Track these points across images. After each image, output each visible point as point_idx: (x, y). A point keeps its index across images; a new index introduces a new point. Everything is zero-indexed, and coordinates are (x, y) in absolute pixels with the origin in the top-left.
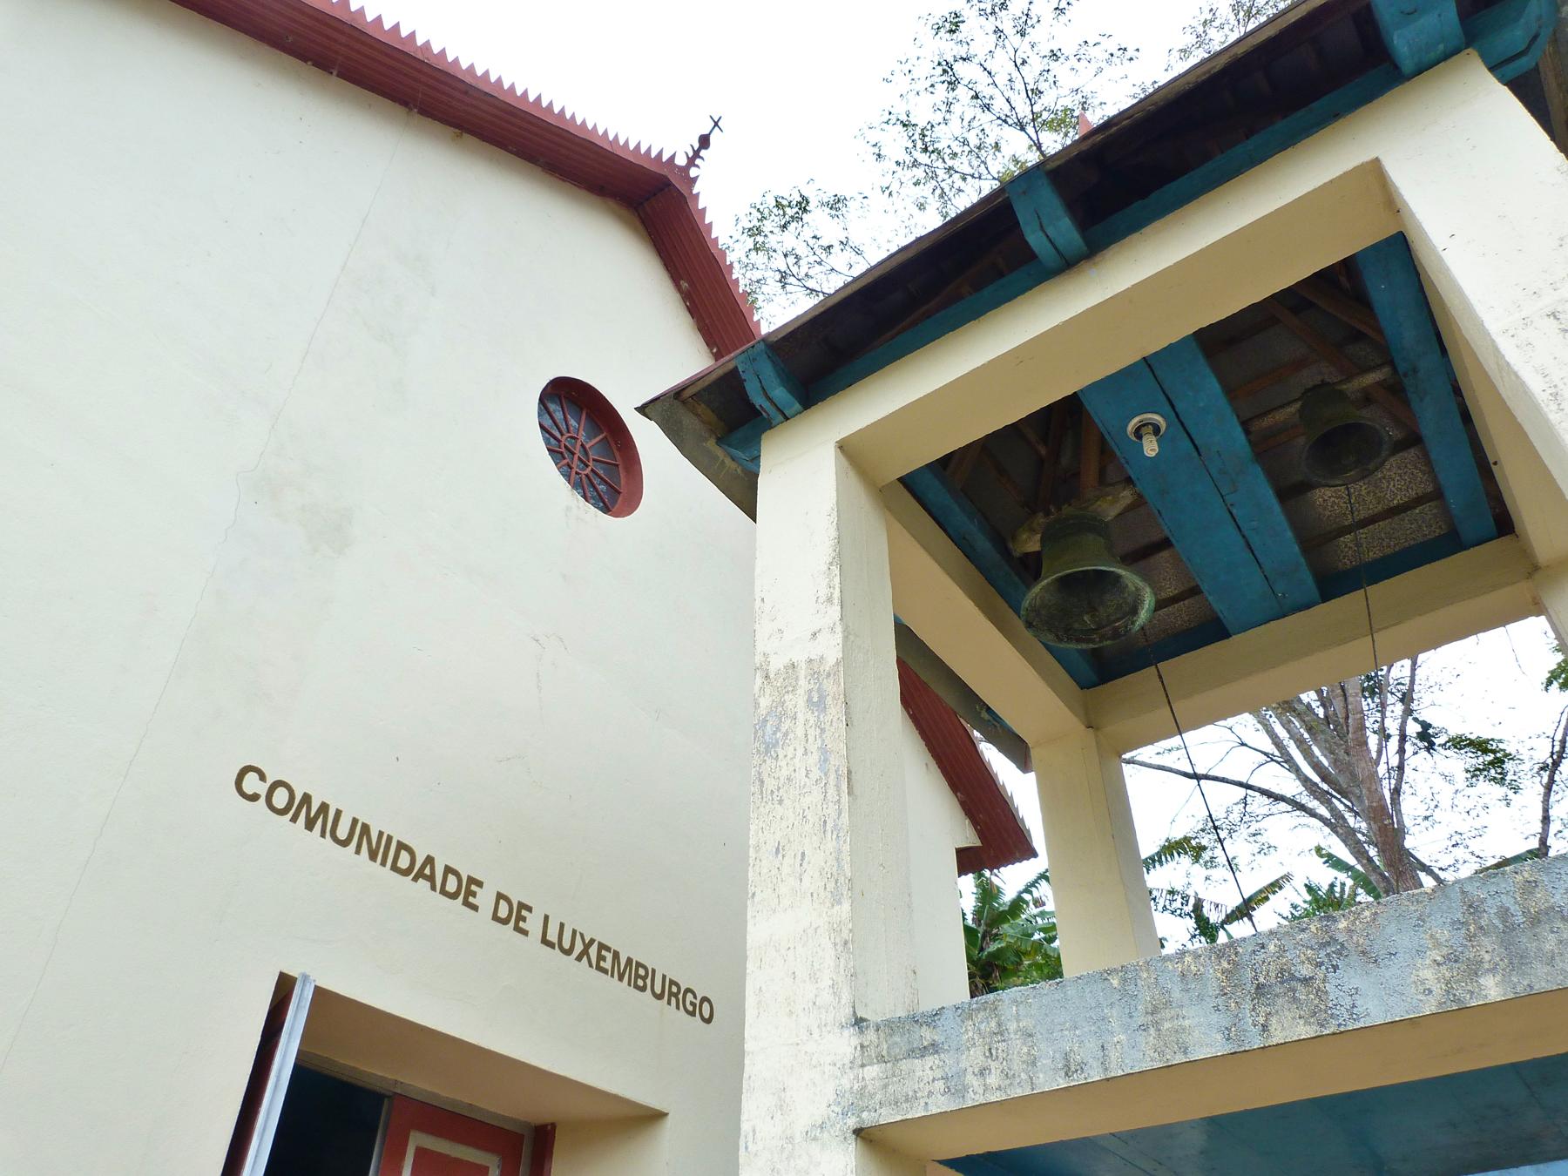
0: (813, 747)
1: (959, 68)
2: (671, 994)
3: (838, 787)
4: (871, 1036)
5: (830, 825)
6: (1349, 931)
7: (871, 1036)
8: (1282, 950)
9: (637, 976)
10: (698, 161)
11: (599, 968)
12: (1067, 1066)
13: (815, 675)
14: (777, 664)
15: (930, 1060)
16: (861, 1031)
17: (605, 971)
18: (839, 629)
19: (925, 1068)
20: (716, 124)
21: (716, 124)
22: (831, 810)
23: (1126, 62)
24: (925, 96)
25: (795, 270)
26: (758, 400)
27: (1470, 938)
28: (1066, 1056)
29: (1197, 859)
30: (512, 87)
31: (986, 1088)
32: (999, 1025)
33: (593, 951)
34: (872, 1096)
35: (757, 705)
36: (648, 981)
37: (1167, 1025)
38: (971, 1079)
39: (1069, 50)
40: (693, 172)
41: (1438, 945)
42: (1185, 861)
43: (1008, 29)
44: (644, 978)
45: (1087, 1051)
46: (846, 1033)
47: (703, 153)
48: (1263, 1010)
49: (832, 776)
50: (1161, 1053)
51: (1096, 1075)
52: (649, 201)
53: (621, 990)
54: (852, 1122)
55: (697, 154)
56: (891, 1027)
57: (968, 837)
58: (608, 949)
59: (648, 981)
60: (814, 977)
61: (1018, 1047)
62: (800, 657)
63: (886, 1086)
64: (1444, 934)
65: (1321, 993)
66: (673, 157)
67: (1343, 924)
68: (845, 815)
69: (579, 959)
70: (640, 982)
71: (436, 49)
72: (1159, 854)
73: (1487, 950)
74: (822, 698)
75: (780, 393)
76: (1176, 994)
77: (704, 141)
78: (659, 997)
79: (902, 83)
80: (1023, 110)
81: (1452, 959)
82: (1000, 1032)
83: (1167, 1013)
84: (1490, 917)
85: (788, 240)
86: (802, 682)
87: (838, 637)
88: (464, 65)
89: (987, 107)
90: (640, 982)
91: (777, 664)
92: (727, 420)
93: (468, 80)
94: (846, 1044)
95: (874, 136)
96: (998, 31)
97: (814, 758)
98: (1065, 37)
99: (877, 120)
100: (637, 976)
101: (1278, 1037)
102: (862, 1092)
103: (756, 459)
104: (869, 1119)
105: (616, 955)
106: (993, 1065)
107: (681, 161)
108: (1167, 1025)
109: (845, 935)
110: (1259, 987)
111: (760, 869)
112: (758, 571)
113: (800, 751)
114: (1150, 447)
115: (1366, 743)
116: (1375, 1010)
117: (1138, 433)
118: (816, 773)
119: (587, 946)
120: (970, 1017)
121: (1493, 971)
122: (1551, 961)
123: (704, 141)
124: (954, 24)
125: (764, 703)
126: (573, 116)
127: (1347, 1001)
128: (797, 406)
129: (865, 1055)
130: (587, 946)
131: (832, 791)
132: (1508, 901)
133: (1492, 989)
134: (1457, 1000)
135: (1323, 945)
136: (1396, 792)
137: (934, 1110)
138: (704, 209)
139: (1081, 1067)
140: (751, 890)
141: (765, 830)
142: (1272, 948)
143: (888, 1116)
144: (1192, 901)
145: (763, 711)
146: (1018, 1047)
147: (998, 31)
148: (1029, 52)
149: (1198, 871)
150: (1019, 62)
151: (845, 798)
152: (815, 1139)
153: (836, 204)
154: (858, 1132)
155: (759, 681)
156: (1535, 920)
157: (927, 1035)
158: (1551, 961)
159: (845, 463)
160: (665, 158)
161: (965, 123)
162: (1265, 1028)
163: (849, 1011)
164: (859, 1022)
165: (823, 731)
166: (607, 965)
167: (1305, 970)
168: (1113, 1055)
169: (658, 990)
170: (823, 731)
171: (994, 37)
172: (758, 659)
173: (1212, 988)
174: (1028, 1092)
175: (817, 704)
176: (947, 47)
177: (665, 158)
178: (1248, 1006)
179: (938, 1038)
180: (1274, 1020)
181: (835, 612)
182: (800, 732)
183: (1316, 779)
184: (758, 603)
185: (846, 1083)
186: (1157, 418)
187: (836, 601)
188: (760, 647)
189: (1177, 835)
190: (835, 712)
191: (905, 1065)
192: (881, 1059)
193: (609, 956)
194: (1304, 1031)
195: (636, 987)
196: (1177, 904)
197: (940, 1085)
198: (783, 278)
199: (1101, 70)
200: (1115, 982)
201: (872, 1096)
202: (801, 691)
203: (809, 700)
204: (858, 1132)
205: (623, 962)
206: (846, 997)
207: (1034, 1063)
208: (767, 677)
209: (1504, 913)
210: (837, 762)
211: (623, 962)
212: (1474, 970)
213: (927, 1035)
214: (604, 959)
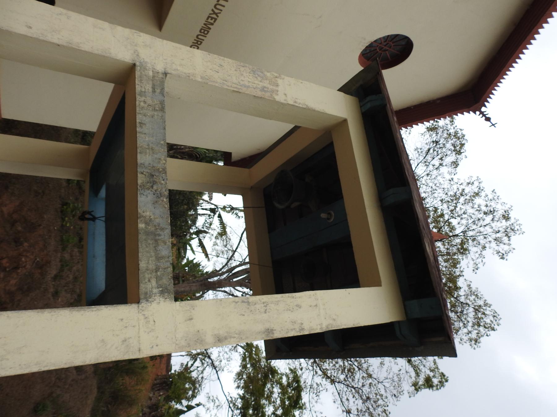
0: (250, 84)
1: (491, 216)
2: (198, 41)
3: (236, 88)
4: (161, 76)
5: (225, 82)
6: (163, 201)
7: (161, 76)
8: (162, 184)
9: (205, 30)
10: (481, 115)
11: (209, 17)
12: (142, 123)
13: (273, 91)
14: (280, 81)
15: (151, 90)
16: (163, 74)
17: (208, 19)
18: (285, 102)
19: (148, 87)
20: (493, 125)
21: (493, 125)
22: (230, 84)
23: (473, 269)
24: (485, 203)
25: (438, 146)
26: (368, 98)
27: (155, 226)
28: (145, 124)
29: (219, 233)
30: (527, 49)
31: (140, 101)
32: (157, 110)
33: (214, 16)
34: (144, 71)
35: (268, 72)
36: (202, 34)
37: (148, 151)
38: (143, 99)
39: (484, 253)
40: (478, 113)
41: (155, 218)
42: (219, 230)
43: (498, 235)
44: (204, 33)
45: (145, 129)
46: (163, 69)
47: (484, 118)
48: (147, 174)
49: (240, 87)
50: (141, 147)
51: (138, 129)
52: (472, 94)
53: (201, 24)
54: (138, 64)
55: (484, 115)
56: (162, 82)
57: (235, 157)
58: (215, 22)
59: (202, 34)
60: (181, 65)
61: (150, 113)
62: (280, 88)
63: (146, 76)
64: (157, 221)
65: (148, 189)
66: (485, 106)
67: (165, 200)
68: (227, 87)
69: (213, 10)
70: (202, 31)
71: (549, 20)
72: (223, 222)
73: (151, 228)
74: (265, 91)
75: (368, 106)
76: (155, 156)
77: (488, 119)
78: (197, 37)
79: (490, 197)
80: (470, 233)
81: (151, 220)
82: (155, 110)
83: (151, 152)
84: (159, 232)
85: (449, 146)
86: (271, 87)
87: (282, 101)
88: (540, 30)
89: (474, 222)
90: (202, 31)
91: (280, 81)
92: (366, 89)
93: (534, 31)
94: (160, 68)
95: (476, 184)
96: (499, 232)
97: (247, 84)
98: (487, 253)
99: (482, 185)
100: (205, 30)
101: (139, 175)
102: (145, 69)
103: (352, 95)
104: (138, 68)
105: (212, 24)
106: (146, 105)
107: (483, 109)
108: (148, 151)
109: (191, 77)
110: (153, 176)
111: (217, 59)
112: (312, 84)
113: (250, 80)
114: (323, 216)
115: (241, 286)
116: (142, 199)
117: (329, 214)
118: (242, 83)
119: (216, 14)
120: (160, 103)
121: (146, 227)
122: (145, 240)
123: (488, 119)
124: (506, 217)
125: (268, 74)
126: (510, 71)
127: (145, 194)
128: (363, 110)
129: (156, 73)
130: (216, 14)
131: (235, 86)
132: (162, 237)
133: (141, 226)
134: (140, 217)
135: (161, 194)
136: (225, 292)
137: (137, 86)
138: (463, 114)
139: (141, 127)
140: (211, 55)
141: (229, 64)
142: (163, 182)
143: (137, 74)
144: (207, 230)
145: (266, 73)
146: (150, 113)
147: (499, 232)
148: (488, 240)
149: (215, 234)
150: (486, 236)
151: (232, 89)
152: (135, 52)
153: (455, 164)
154: (134, 65)
155: (276, 75)
156: (156, 241)
157: (158, 91)
158: (145, 240)
159: (340, 120)
160: (486, 103)
161: (471, 215)
162: (142, 173)
163: (169, 72)
164: (166, 74)
165: (255, 88)
166: (209, 20)
167: (155, 187)
168: (143, 136)
169: (200, 37)
170: (255, 88)
171: (497, 230)
172: (283, 76)
173: (155, 165)
174: (137, 111)
175: (263, 89)
176: (498, 214)
177: (486, 103)
178: (149, 171)
179: (156, 94)
180: (144, 176)
181: (291, 103)
182: (256, 82)
183: (233, 272)
184: (301, 81)
185: (149, 65)
186: (332, 220)
187: (294, 104)
188: (286, 78)
189: (228, 230)
190: (259, 94)
191: (151, 82)
192: (154, 77)
193: (212, 21)
194: (140, 182)
195: (201, 29)
196: (207, 225)
197: (143, 90)
198: (437, 142)
199: (473, 260)
200: (162, 142)
201: (144, 71)
202: (269, 86)
203: (265, 87)
204: (134, 65)
205: (209, 26)
206: (173, 72)
207: (144, 115)
208: (276, 77)
209: (159, 235)
210: (244, 90)
211: (209, 26)
212: (147, 223)
213: (158, 91)
214: (212, 19)
